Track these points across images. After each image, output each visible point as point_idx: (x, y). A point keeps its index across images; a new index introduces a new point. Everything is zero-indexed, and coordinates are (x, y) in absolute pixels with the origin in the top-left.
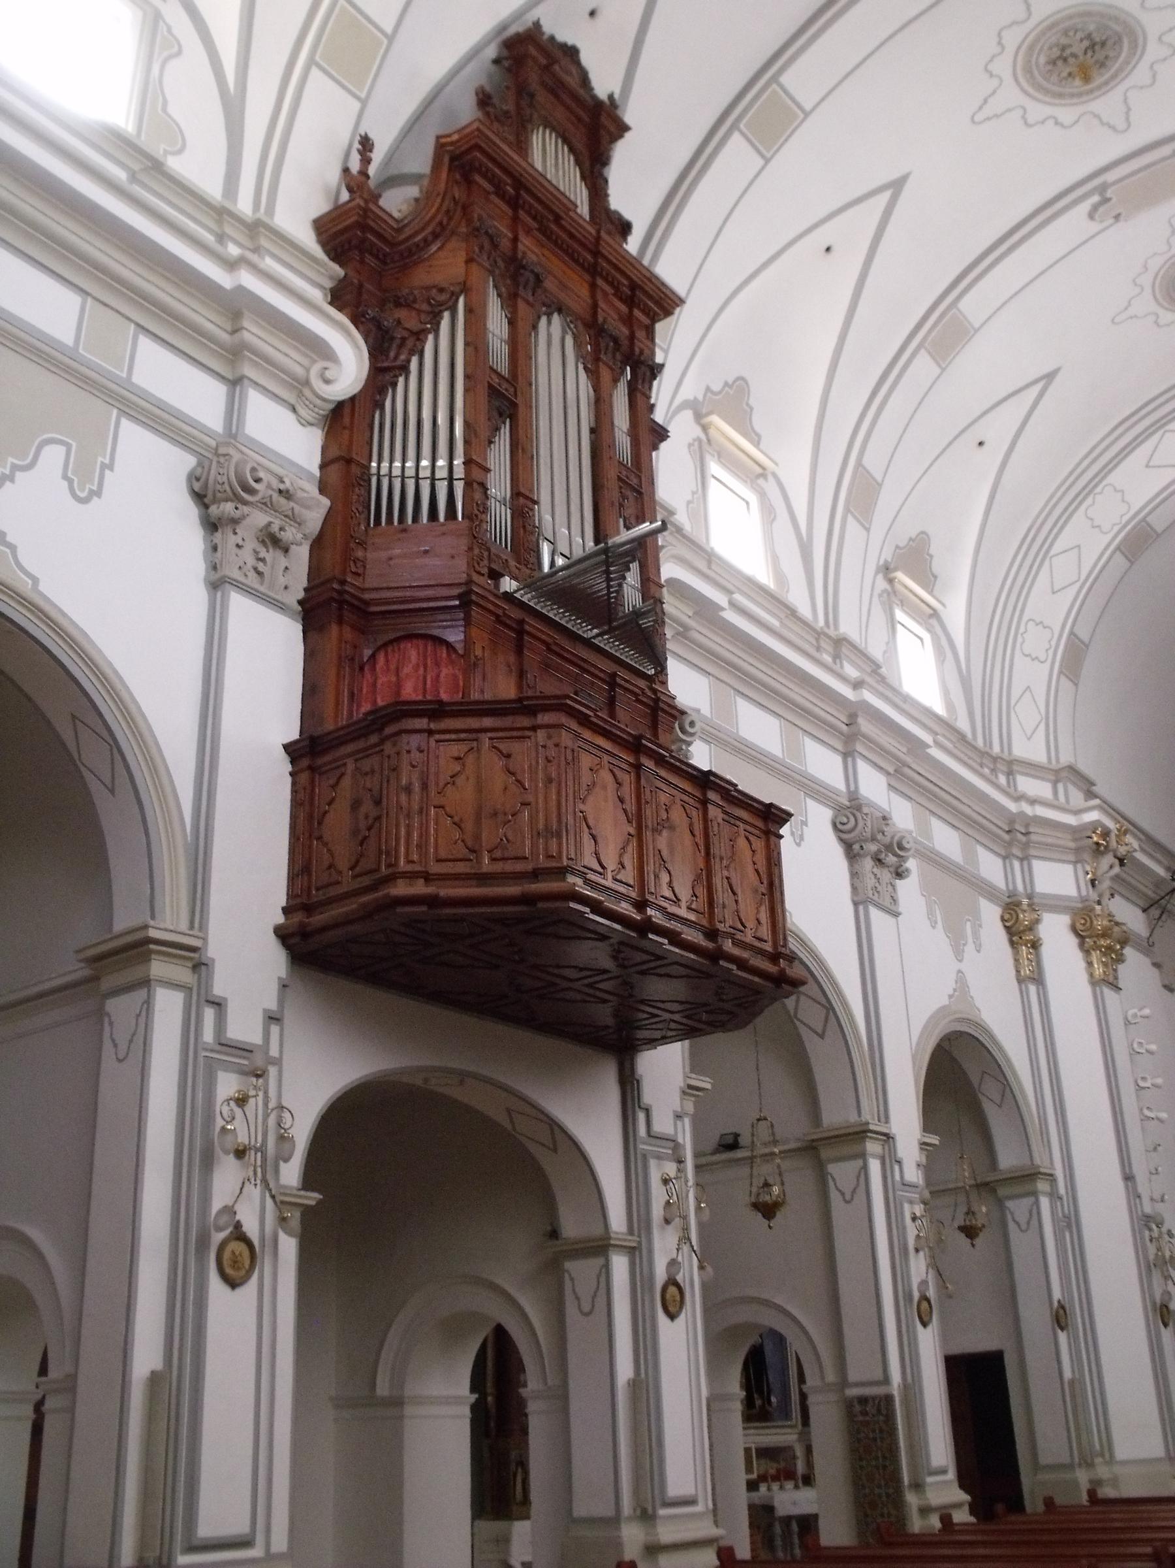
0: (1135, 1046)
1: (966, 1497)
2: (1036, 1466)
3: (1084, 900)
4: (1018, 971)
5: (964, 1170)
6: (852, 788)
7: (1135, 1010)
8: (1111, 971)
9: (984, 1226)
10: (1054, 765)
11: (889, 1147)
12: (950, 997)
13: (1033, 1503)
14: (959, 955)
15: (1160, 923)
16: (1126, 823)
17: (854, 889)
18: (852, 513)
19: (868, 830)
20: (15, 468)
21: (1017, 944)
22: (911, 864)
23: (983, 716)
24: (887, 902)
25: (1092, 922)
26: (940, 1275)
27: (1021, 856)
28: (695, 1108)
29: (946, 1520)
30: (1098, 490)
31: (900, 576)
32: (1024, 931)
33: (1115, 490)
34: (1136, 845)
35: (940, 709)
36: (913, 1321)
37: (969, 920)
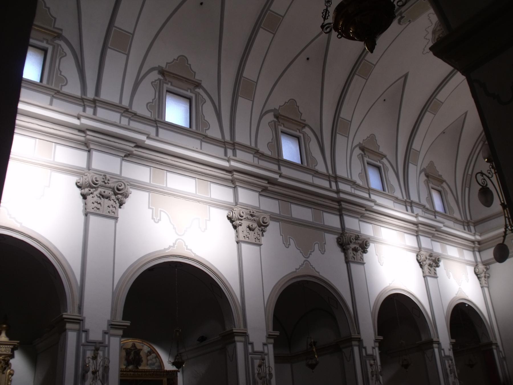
20: (311, 252)
28: (379, 345)
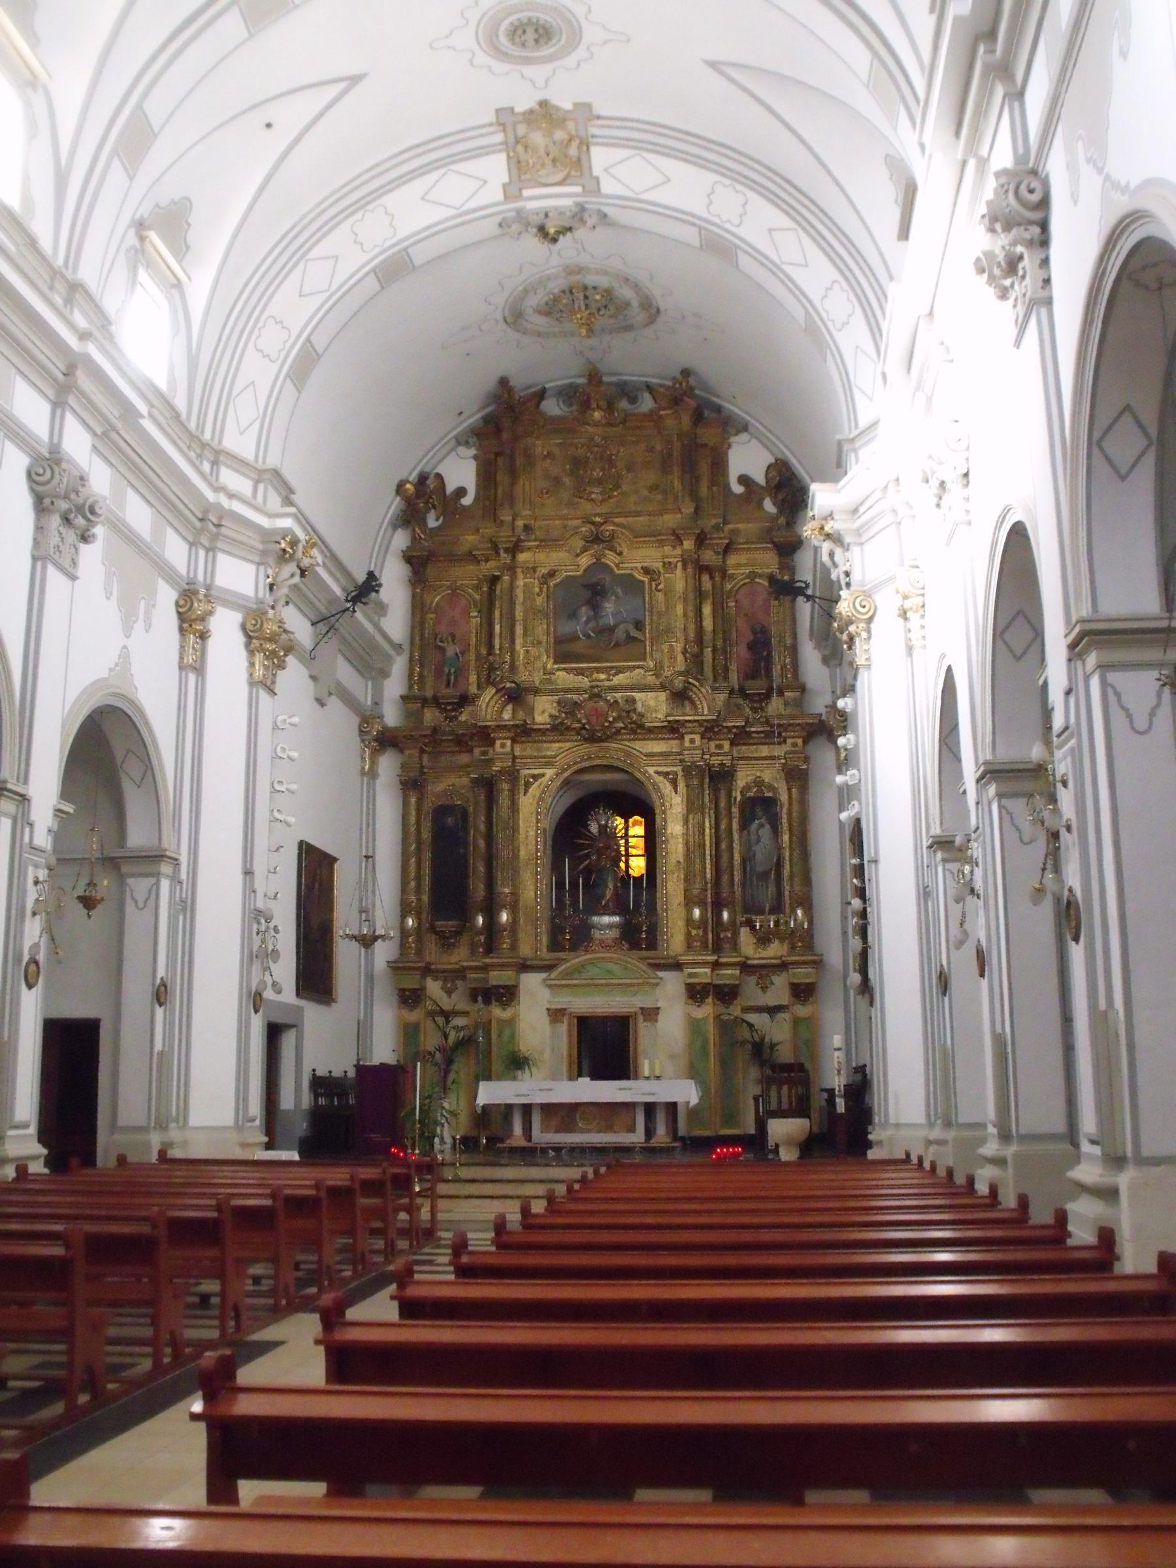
0: (279, 750)
1: (45, 1151)
2: (113, 1127)
3: (260, 602)
4: (181, 658)
5: (92, 842)
6: (55, 441)
7: (286, 717)
8: (271, 676)
9: (102, 899)
10: (260, 465)
11: (23, 808)
12: (111, 670)
13: (105, 1157)
14: (128, 631)
15: (326, 639)
16: (316, 537)
17: (36, 543)
18: (119, 156)
19: (63, 486)
21: (186, 631)
22: (99, 531)
23: (202, 401)
24: (67, 563)
25: (262, 625)
26: (53, 940)
27: (191, 540)
29: (22, 1170)
30: (370, 207)
31: (153, 236)
32: (195, 620)
33: (386, 213)
34: (320, 560)
35: (163, 385)
36: (19, 981)
37: (143, 598)
